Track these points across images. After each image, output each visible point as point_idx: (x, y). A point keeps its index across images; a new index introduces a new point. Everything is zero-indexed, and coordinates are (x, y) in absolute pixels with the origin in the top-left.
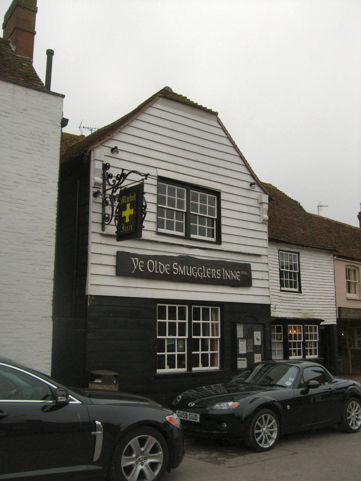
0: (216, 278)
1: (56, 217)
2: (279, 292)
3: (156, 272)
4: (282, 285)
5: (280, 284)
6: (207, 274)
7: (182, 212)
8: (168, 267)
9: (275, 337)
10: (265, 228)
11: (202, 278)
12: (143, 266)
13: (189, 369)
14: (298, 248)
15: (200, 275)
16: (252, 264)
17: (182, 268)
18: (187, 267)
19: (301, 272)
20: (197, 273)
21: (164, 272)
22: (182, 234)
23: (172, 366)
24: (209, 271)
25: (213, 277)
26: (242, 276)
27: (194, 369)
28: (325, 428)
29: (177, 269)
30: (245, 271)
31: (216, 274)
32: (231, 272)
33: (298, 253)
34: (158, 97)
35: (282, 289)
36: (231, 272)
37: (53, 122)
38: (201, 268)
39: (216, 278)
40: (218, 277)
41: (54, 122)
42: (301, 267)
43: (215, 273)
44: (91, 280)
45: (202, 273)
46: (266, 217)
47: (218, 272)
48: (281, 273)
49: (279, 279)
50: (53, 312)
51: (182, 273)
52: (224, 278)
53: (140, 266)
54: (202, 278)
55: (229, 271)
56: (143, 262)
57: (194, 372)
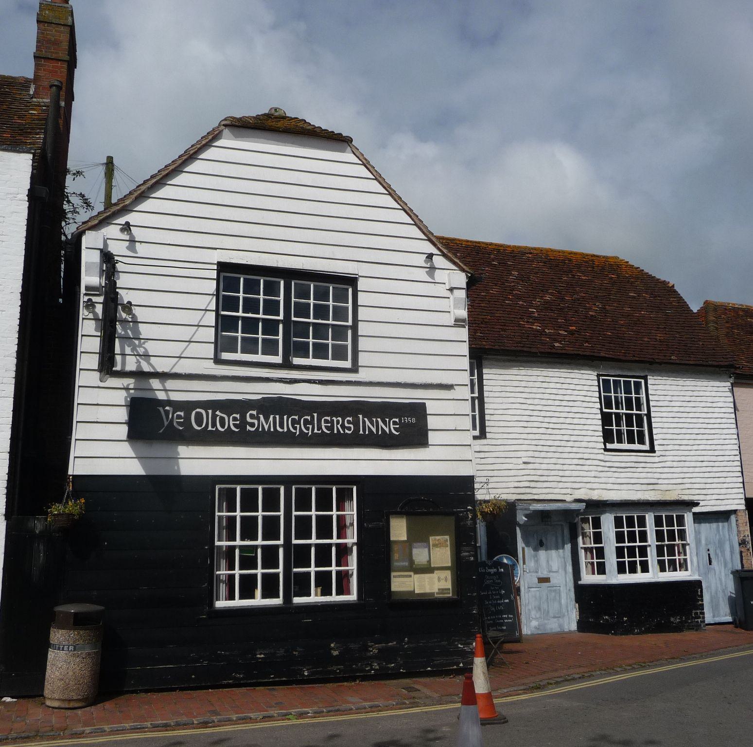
0: (342, 432)
1: (16, 349)
2: (602, 453)
3: (210, 428)
4: (608, 437)
5: (604, 437)
8: (235, 419)
9: (591, 542)
10: (463, 333)
11: (310, 434)
12: (398, 426)
13: (287, 598)
14: (643, 369)
15: (308, 429)
16: (428, 404)
17: (267, 419)
18: (277, 417)
20: (300, 427)
21: (226, 427)
24: (326, 421)
25: (335, 432)
26: (402, 427)
27: (297, 600)
28: (350, 689)
31: (343, 426)
32: (379, 420)
35: (609, 446)
36: (379, 420)
37: (12, 196)
38: (309, 418)
39: (342, 432)
40: (347, 431)
42: (652, 404)
43: (341, 424)
44: (77, 449)
45: (311, 426)
47: (349, 422)
48: (606, 419)
49: (600, 428)
51: (266, 427)
52: (361, 432)
54: (310, 434)
56: (351, 419)
57: (294, 605)
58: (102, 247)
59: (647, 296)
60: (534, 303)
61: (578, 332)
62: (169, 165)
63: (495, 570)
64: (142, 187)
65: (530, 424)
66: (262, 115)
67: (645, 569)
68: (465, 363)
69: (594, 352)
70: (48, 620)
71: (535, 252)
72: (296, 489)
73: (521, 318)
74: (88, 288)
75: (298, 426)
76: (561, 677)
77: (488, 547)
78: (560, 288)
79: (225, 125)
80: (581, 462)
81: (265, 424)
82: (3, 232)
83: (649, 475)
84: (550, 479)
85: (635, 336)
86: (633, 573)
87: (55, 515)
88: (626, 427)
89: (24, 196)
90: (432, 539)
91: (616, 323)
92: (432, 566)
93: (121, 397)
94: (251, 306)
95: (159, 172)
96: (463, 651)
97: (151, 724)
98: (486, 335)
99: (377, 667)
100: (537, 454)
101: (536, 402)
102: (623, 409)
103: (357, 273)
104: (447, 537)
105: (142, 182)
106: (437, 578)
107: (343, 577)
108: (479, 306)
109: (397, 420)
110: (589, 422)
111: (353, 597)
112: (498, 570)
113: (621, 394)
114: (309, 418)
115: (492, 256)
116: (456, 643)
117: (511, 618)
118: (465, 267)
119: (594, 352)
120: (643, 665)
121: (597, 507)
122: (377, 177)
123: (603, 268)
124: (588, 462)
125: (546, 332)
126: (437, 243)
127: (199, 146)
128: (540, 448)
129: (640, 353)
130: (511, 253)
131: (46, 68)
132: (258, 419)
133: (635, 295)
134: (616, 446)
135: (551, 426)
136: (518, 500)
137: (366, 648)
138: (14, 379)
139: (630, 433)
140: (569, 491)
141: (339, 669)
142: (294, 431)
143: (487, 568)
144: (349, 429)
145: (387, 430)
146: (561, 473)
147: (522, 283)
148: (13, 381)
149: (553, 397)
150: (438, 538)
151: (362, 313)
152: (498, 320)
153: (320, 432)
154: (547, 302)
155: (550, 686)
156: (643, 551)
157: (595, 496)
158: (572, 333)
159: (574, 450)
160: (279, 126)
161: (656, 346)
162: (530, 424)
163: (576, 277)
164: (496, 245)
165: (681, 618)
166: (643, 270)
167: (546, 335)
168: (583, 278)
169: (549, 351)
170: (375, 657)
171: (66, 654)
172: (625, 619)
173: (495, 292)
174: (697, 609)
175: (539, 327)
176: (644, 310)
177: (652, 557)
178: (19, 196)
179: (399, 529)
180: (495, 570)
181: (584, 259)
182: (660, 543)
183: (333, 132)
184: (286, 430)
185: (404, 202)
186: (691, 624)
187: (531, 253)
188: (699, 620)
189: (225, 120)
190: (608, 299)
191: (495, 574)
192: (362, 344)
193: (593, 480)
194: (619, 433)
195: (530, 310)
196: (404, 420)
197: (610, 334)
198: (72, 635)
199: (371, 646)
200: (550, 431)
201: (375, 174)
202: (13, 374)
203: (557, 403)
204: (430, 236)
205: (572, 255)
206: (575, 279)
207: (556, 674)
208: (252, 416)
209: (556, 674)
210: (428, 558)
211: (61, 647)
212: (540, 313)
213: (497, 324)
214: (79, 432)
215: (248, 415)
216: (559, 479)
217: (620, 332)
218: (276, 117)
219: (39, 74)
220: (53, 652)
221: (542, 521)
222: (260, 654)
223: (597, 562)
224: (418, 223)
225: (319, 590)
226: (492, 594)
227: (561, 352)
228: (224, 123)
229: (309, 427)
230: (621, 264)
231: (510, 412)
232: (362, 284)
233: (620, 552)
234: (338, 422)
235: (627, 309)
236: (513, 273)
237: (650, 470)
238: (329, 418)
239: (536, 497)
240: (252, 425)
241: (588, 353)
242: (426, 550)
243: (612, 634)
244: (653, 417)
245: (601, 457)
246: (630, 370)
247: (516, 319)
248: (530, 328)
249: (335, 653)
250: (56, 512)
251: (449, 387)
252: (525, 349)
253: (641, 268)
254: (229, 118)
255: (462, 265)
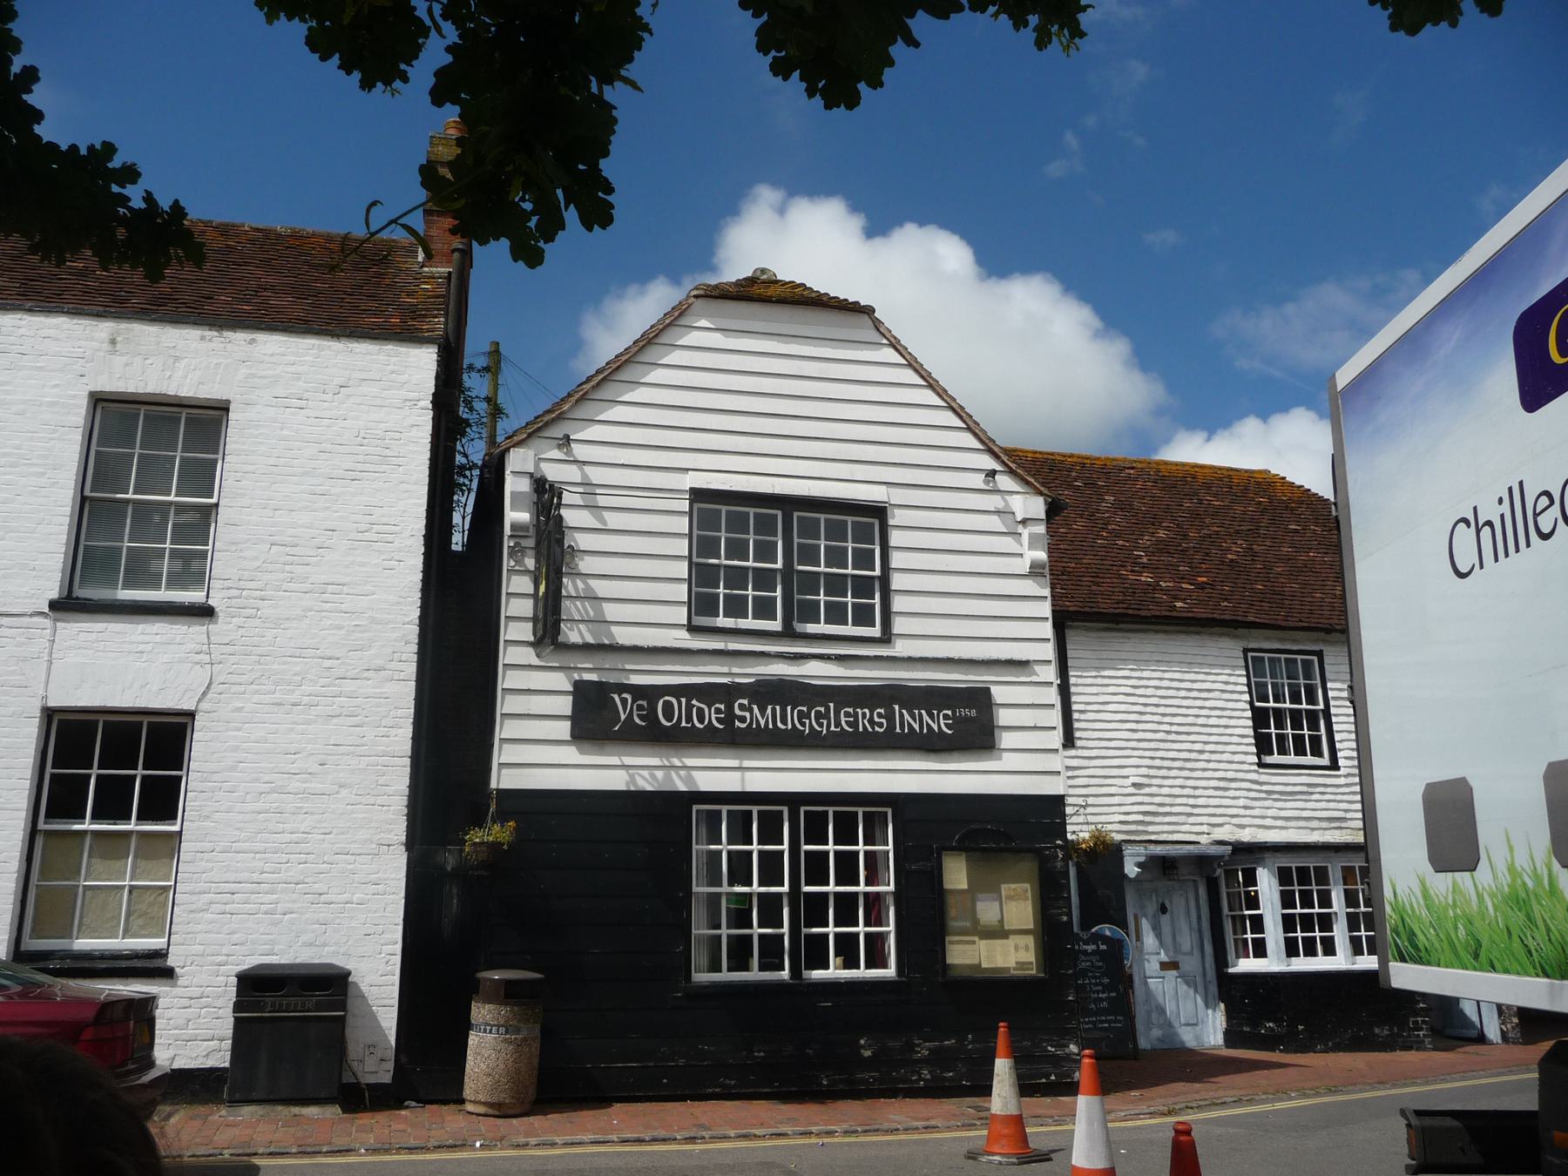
0: (870, 730)
1: (419, 614)
3: (684, 724)
4: (1263, 745)
5: (1257, 745)
6: (843, 723)
7: (872, 578)
8: (718, 711)
11: (825, 732)
12: (951, 722)
14: (1316, 641)
15: (821, 725)
16: (994, 690)
17: (763, 711)
18: (778, 708)
19: (1332, 708)
21: (706, 723)
22: (776, 625)
23: (851, 963)
24: (847, 715)
25: (861, 729)
26: (957, 723)
29: (748, 715)
30: (970, 708)
31: (871, 721)
32: (923, 712)
33: (1320, 654)
34: (693, 300)
35: (1268, 759)
36: (923, 712)
37: (412, 403)
38: (822, 709)
39: (870, 730)
40: (877, 729)
41: (415, 403)
43: (869, 719)
44: (502, 754)
45: (825, 722)
46: (1042, 555)
47: (880, 715)
49: (1251, 732)
50: (407, 831)
51: (762, 723)
52: (898, 730)
53: (635, 713)
54: (825, 732)
55: (917, 712)
56: (882, 711)
58: (532, 471)
59: (1317, 528)
60: (1141, 542)
61: (1211, 585)
62: (621, 354)
63: (1094, 947)
64: (584, 386)
65: (1141, 726)
66: (744, 279)
67: (1329, 949)
68: (1047, 630)
69: (1238, 615)
70: (469, 990)
71: (1139, 465)
72: (805, 812)
73: (1122, 566)
74: (514, 527)
75: (807, 721)
76: (1205, 1100)
77: (1081, 913)
78: (1180, 519)
79: (696, 297)
80: (1222, 784)
81: (760, 718)
82: (399, 452)
83: (1332, 805)
84: (1175, 809)
85: (1300, 590)
86: (1312, 956)
87: (475, 844)
88: (1292, 730)
89: (427, 403)
90: (1006, 889)
91: (1269, 571)
92: (1006, 928)
93: (561, 681)
94: (737, 550)
95: (607, 364)
96: (1054, 1056)
97: (618, 1138)
98: (1070, 591)
99: (928, 1077)
100: (1152, 772)
101: (1150, 692)
102: (1285, 702)
103: (887, 500)
104: (1027, 886)
105: (585, 380)
106: (1013, 945)
107: (875, 942)
108: (1058, 549)
109: (949, 713)
110: (1232, 722)
111: (890, 972)
112: (1098, 947)
113: (1282, 678)
114: (822, 709)
115: (1074, 474)
116: (1045, 1044)
117: (1120, 1022)
118: (1042, 489)
119: (1238, 615)
120: (1333, 1089)
121: (1249, 854)
122: (912, 362)
123: (1246, 488)
124: (1234, 785)
125: (1161, 586)
126: (1001, 455)
127: (661, 327)
128: (1158, 763)
129: (1309, 615)
130: (1103, 469)
131: (440, 225)
132: (751, 711)
133: (1298, 528)
134: (1275, 758)
135: (1174, 728)
136: (1123, 841)
137: (911, 1048)
138: (416, 656)
139: (1299, 740)
140: (1205, 829)
141: (872, 1077)
142: (802, 729)
143: (1081, 944)
144: (881, 725)
145: (935, 727)
146: (1191, 801)
147: (1121, 513)
148: (415, 658)
149: (1175, 684)
150: (1013, 886)
151: (897, 560)
152: (1087, 568)
153: (839, 730)
154: (1161, 541)
155: (1190, 1111)
156: (1326, 922)
157: (1246, 836)
158: (1201, 587)
159: (1212, 765)
160: (769, 294)
161: (1335, 605)
162: (1141, 726)
163: (1205, 502)
164: (1079, 457)
165: (1391, 1030)
166: (1309, 490)
167: (1162, 590)
168: (1216, 503)
169: (1168, 613)
170: (925, 1061)
171: (495, 1038)
172: (1301, 1027)
173: (1080, 528)
174: (1416, 1016)
175: (1151, 578)
176: (1312, 550)
177: (1340, 933)
178: (422, 404)
179: (956, 874)
180: (1094, 947)
181: (1216, 475)
182: (1352, 910)
183: (846, 300)
184: (790, 727)
185: (951, 397)
186: (1408, 1039)
187: (1133, 468)
188: (1421, 1033)
189: (696, 288)
190: (1256, 535)
191: (1094, 953)
192: (898, 604)
193: (1242, 812)
194: (1281, 739)
195: (1135, 553)
196: (960, 712)
197: (1261, 587)
198: (503, 1012)
199: (918, 1045)
200: (1173, 737)
201: (908, 357)
202: (415, 648)
203: (1183, 693)
204: (990, 444)
205: (1197, 469)
206: (1203, 506)
207: (1197, 1096)
208: (742, 707)
209: (1197, 1096)
210: (1000, 917)
211: (488, 1028)
212: (1151, 558)
213: (1086, 574)
214: (505, 730)
215: (736, 705)
216: (1188, 810)
217: (1276, 584)
218: (764, 282)
219: (432, 234)
220: (476, 1035)
221: (1164, 874)
222: (759, 1051)
223: (1252, 938)
224: (972, 427)
225: (840, 960)
226: (1090, 984)
227: (1185, 615)
228: (695, 292)
229: (823, 723)
230: (1274, 480)
231: (1110, 707)
232: (896, 518)
233: (1288, 923)
234: (864, 715)
235: (1286, 549)
236: (1107, 497)
237: (1332, 797)
238: (851, 710)
239: (1153, 837)
240: (743, 720)
241: (1227, 617)
242: (997, 904)
243: (1281, 1051)
244: (1334, 715)
245: (1254, 776)
246: (1295, 641)
247: (1115, 568)
248: (1137, 580)
249: (867, 1053)
250: (477, 840)
251: (1022, 665)
252: (1130, 612)
253: (1307, 487)
254: (702, 287)
255: (1038, 486)
